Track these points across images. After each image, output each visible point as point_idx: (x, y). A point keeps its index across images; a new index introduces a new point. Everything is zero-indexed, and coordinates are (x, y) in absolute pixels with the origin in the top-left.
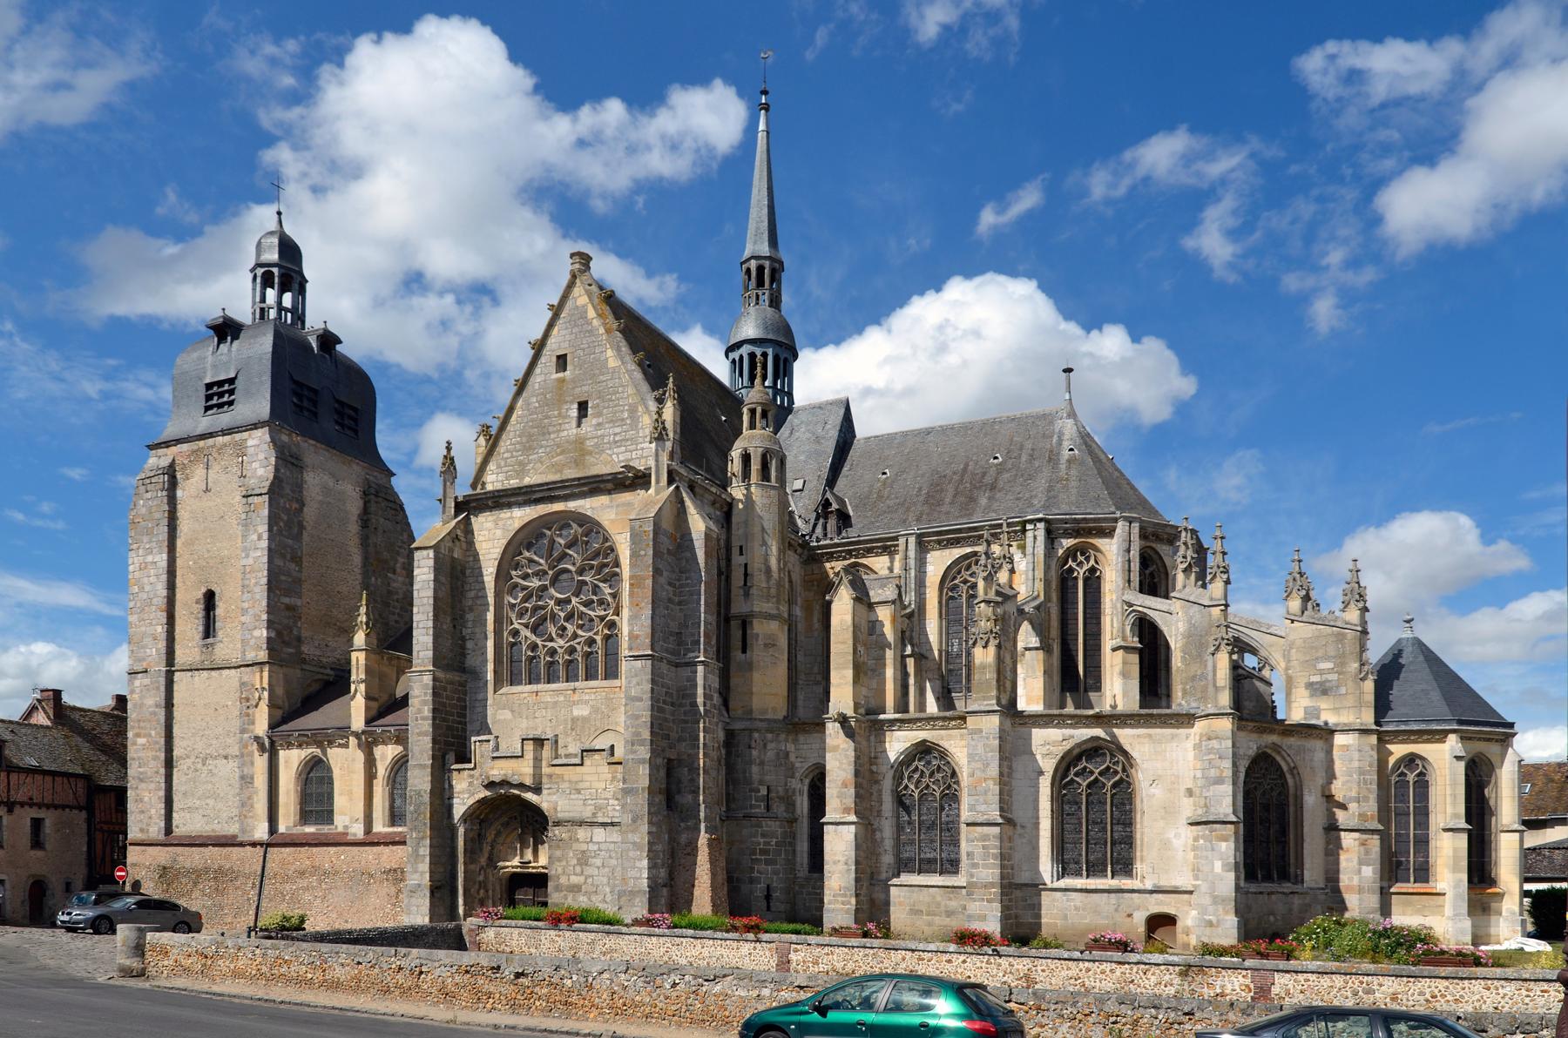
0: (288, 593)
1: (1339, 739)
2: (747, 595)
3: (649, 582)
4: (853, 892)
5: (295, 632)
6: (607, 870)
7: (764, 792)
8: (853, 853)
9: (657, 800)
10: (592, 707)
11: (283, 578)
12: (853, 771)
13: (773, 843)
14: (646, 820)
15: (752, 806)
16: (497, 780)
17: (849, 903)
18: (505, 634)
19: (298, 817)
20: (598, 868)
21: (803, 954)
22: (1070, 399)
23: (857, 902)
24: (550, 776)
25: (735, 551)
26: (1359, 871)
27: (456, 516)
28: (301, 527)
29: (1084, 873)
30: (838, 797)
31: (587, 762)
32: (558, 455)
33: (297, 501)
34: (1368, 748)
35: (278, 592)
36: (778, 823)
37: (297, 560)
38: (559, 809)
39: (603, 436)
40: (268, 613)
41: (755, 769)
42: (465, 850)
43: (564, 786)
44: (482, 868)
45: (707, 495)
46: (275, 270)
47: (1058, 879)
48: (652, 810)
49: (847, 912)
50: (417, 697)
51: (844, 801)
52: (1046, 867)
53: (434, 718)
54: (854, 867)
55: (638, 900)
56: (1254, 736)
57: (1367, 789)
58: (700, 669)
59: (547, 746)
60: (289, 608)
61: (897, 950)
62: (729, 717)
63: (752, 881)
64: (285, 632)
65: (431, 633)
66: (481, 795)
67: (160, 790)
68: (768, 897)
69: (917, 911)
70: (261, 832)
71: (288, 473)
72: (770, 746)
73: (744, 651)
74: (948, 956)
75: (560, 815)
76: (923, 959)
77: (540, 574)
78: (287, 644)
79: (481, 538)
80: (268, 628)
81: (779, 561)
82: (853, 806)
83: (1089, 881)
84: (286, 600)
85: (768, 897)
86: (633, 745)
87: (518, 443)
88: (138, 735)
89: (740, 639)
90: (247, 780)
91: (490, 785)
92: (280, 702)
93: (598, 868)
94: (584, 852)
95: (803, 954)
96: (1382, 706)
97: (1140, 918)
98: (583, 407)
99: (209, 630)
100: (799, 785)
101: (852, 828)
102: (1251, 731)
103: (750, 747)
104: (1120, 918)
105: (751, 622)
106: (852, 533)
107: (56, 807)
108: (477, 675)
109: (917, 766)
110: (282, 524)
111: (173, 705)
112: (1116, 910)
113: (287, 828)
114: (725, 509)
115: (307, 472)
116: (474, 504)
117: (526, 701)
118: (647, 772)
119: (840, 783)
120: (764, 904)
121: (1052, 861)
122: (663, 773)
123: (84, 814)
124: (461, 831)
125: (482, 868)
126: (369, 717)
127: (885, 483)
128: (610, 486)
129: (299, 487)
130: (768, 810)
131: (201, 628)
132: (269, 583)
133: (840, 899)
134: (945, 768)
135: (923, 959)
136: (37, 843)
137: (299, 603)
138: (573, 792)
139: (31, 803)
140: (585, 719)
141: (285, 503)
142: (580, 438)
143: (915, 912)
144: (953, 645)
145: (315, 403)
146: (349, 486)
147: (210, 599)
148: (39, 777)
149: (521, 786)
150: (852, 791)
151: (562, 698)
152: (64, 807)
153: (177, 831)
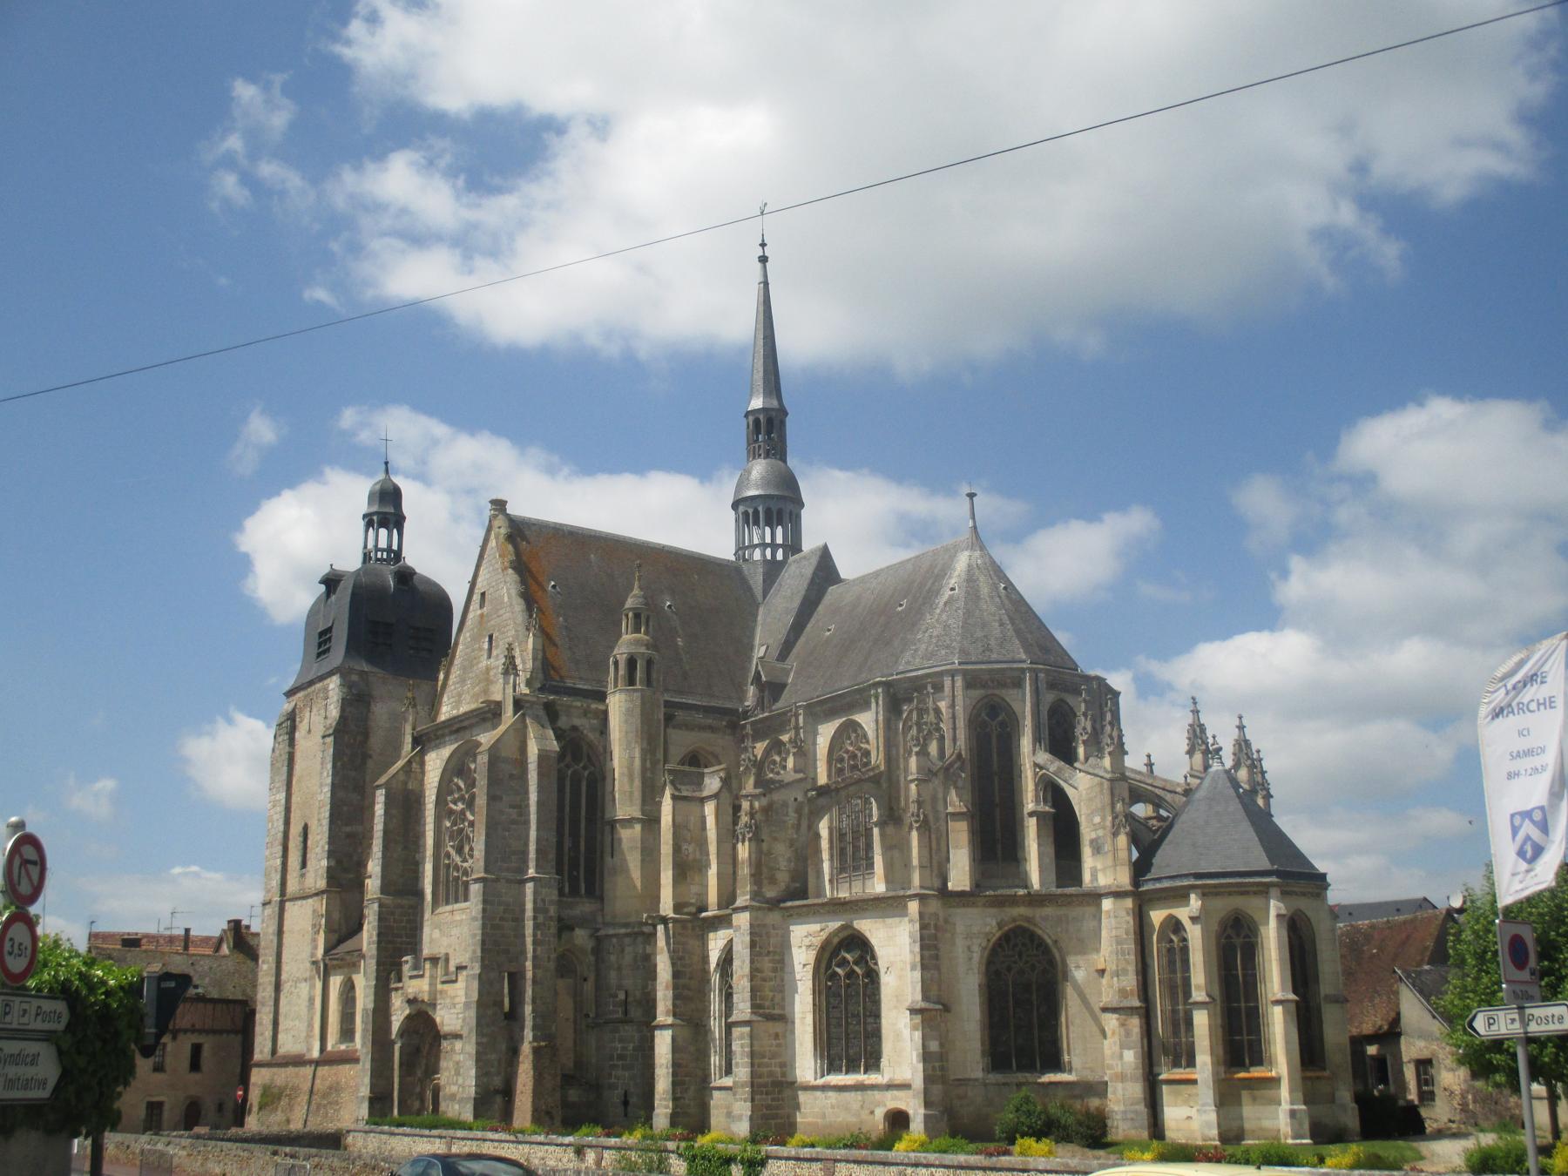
1: (1107, 904)
5: (355, 858)
7: (622, 996)
8: (670, 1056)
11: (345, 808)
22: (975, 527)
24: (441, 992)
26: (1121, 1056)
27: (515, 715)
29: (844, 1069)
34: (1123, 913)
35: (339, 822)
36: (635, 1027)
41: (613, 974)
44: (419, 1080)
47: (823, 1076)
52: (806, 1066)
56: (993, 911)
57: (1125, 959)
58: (529, 887)
59: (441, 964)
60: (349, 836)
63: (612, 1087)
66: (407, 1012)
68: (626, 1103)
70: (316, 1054)
72: (628, 950)
79: (430, 768)
80: (328, 858)
81: (643, 760)
83: (848, 1077)
84: (348, 829)
85: (626, 1103)
88: (263, 962)
96: (1140, 869)
97: (880, 1113)
98: (491, 637)
102: (984, 905)
104: (865, 1115)
107: (214, 1032)
108: (420, 894)
112: (862, 1107)
113: (333, 1047)
120: (620, 1110)
121: (815, 1055)
123: (239, 1038)
124: (397, 1047)
125: (419, 1080)
126: (355, 939)
132: (331, 815)
136: (195, 1065)
139: (193, 1030)
147: (306, 829)
148: (201, 1005)
152: (220, 1032)
153: (281, 1051)
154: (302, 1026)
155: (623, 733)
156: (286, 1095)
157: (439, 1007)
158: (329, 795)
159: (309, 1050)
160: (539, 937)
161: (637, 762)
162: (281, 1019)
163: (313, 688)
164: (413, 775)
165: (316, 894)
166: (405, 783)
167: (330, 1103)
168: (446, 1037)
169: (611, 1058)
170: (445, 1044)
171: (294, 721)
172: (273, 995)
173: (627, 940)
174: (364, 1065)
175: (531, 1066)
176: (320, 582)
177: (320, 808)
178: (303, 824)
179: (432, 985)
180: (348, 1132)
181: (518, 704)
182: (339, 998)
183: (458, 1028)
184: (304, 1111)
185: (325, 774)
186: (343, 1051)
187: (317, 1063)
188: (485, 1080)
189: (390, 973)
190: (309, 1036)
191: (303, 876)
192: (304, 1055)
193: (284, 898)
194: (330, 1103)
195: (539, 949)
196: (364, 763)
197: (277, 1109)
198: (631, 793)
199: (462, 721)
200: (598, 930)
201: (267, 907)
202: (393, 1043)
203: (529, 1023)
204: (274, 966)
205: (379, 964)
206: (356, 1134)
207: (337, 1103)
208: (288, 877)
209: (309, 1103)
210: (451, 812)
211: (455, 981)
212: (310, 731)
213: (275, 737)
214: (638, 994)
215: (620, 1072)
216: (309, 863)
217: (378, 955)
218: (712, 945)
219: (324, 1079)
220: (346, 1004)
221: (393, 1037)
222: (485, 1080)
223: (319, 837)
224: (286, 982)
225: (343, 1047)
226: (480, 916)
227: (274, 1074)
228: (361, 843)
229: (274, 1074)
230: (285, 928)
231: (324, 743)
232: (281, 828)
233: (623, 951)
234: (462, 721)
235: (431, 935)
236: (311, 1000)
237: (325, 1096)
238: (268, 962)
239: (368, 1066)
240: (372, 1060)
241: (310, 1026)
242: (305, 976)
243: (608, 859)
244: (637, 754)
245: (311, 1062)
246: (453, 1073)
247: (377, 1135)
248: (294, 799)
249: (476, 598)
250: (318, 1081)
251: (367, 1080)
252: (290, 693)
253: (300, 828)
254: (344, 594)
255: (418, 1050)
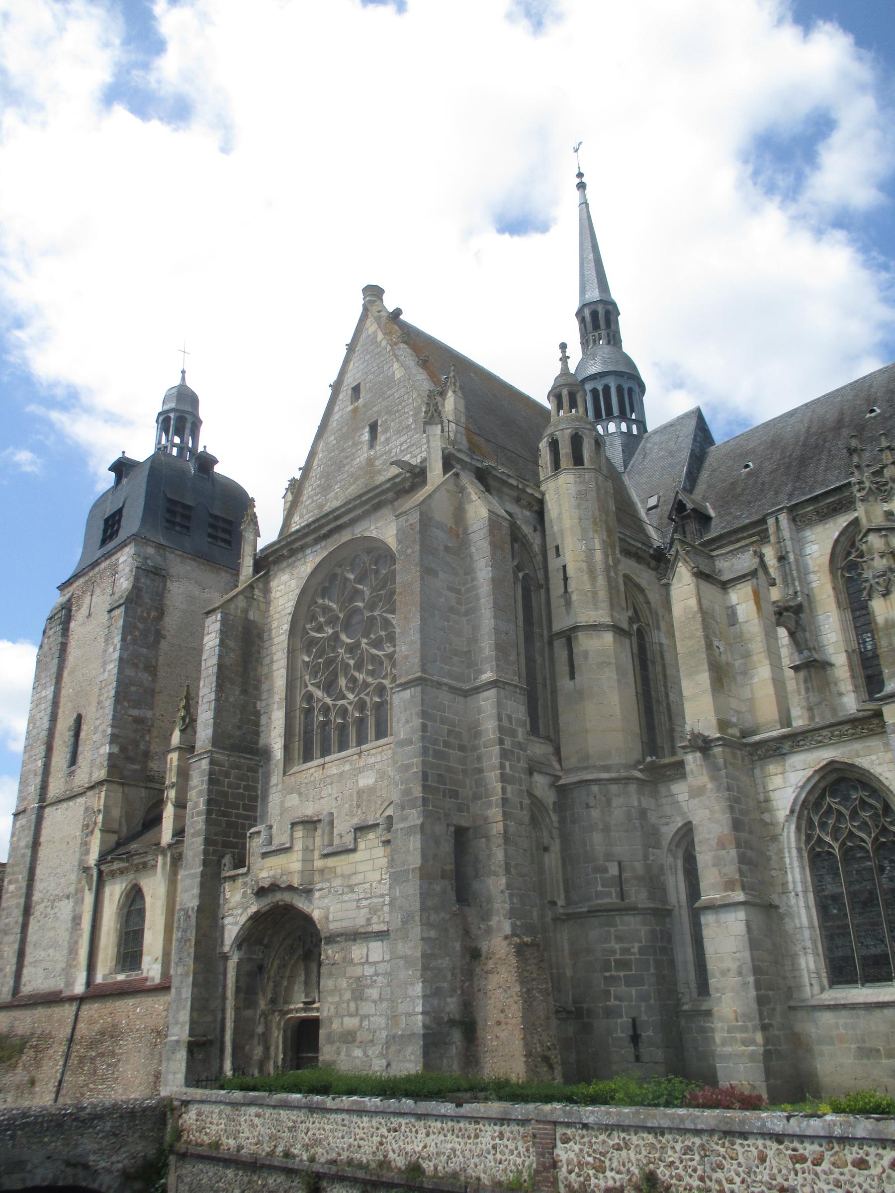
0: (137, 704)
2: (568, 603)
3: (417, 586)
4: (757, 1022)
5: (142, 747)
6: (385, 1005)
7: (613, 870)
8: (747, 954)
9: (438, 888)
10: (378, 771)
11: (133, 689)
12: (730, 823)
13: (636, 950)
14: (417, 918)
15: (598, 895)
16: (266, 884)
17: (753, 1042)
18: (298, 699)
19: (114, 963)
20: (375, 1002)
21: (576, 1148)
23: (767, 1041)
24: (322, 871)
25: (551, 553)
28: (159, 636)
30: (714, 865)
31: (362, 845)
32: (352, 485)
33: (156, 609)
35: (126, 704)
37: (151, 669)
38: (331, 917)
39: (390, 451)
40: (112, 726)
41: (597, 838)
42: (238, 990)
43: (337, 882)
45: (506, 490)
46: (172, 415)
48: (430, 903)
49: (752, 1057)
50: (195, 787)
51: (724, 871)
53: (209, 812)
54: (751, 979)
55: (409, 1049)
60: (138, 720)
61: (744, 1135)
62: (562, 769)
63: (610, 1013)
64: (130, 747)
65: (213, 707)
66: (254, 909)
67: (14, 942)
68: (635, 1039)
69: (871, 1050)
71: (148, 582)
72: (616, 802)
73: (572, 677)
74: (852, 1153)
75: (334, 926)
76: (803, 1159)
77: (332, 621)
78: (132, 760)
80: (111, 743)
81: (606, 556)
82: (737, 876)
84: (135, 712)
85: (635, 1039)
86: (403, 809)
87: (318, 486)
88: (10, 882)
89: (567, 664)
90: (76, 920)
91: (261, 892)
92: (116, 826)
93: (375, 1002)
94: (358, 979)
95: (576, 1148)
98: (373, 428)
99: (73, 760)
100: (671, 859)
101: (741, 915)
103: (588, 806)
105: (577, 638)
106: (715, 531)
108: (265, 754)
109: (830, 807)
110: (137, 633)
111: (40, 844)
113: (105, 977)
114: (536, 508)
115: (172, 581)
116: (271, 559)
117: (312, 779)
118: (418, 845)
119: (714, 843)
120: (628, 1050)
122: (447, 847)
124: (232, 964)
126: (155, 830)
127: (749, 474)
128: (390, 495)
129: (159, 597)
130: (623, 899)
131: (68, 756)
133: (738, 1035)
134: (871, 801)
135: (803, 1159)
137: (149, 714)
138: (346, 890)
140: (371, 790)
141: (143, 611)
142: (370, 460)
143: (867, 1053)
144: (865, 642)
145: (188, 518)
146: (216, 594)
147: (79, 720)
149: (290, 888)
150: (733, 852)
151: (347, 767)
153: (27, 989)
154: (59, 957)
155: (576, 521)
156: (32, 1047)
157: (317, 894)
158: (115, 671)
159: (70, 984)
160: (508, 770)
161: (599, 556)
162: (29, 950)
163: (97, 570)
164: (255, 603)
165: (91, 788)
166: (246, 611)
167: (102, 1055)
168: (332, 939)
169: (607, 966)
170: (329, 952)
171: (70, 610)
172: (21, 919)
173: (614, 788)
174: (179, 993)
175: (513, 978)
176: (111, 469)
177: (100, 689)
178: (75, 716)
179: (307, 860)
180: (186, 1103)
181: (448, 463)
182: (118, 914)
183: (361, 921)
184: (59, 1068)
185: (111, 650)
186: (122, 982)
187: (81, 1000)
188: (436, 1002)
189: (223, 856)
190: (70, 965)
191: (71, 774)
192: (61, 992)
193: (43, 802)
194: (102, 1055)
195: (509, 788)
196: (157, 642)
197: (16, 1066)
198: (595, 593)
199: (336, 518)
200: (559, 778)
201: (20, 817)
202: (225, 957)
203: (501, 905)
204: (24, 884)
205: (208, 842)
206: (206, 1108)
207: (113, 1054)
208: (51, 780)
209: (67, 1056)
210: (313, 642)
211: (354, 850)
212: (90, 615)
213: (44, 632)
214: (639, 866)
215: (623, 989)
216: (80, 759)
217: (207, 830)
218: (776, 781)
219: (91, 1022)
220: (127, 921)
221: (226, 949)
222: (436, 1002)
223: (98, 722)
224: (38, 903)
225: (121, 977)
226: (416, 737)
227: (16, 1019)
228: (149, 731)
229: (16, 1019)
230: (42, 839)
231: (111, 618)
232: (46, 725)
233: (609, 802)
234: (336, 518)
235: (282, 802)
236: (76, 920)
237: (93, 1044)
238: (17, 881)
239: (187, 993)
240: (194, 984)
241: (73, 951)
242: (66, 891)
243: (565, 684)
244: (597, 546)
245: (72, 999)
246: (348, 995)
247: (268, 1112)
248: (64, 692)
249: (345, 394)
250: (81, 1025)
251: (185, 1016)
252: (62, 587)
253: (71, 721)
254: (138, 484)
255: (261, 968)
